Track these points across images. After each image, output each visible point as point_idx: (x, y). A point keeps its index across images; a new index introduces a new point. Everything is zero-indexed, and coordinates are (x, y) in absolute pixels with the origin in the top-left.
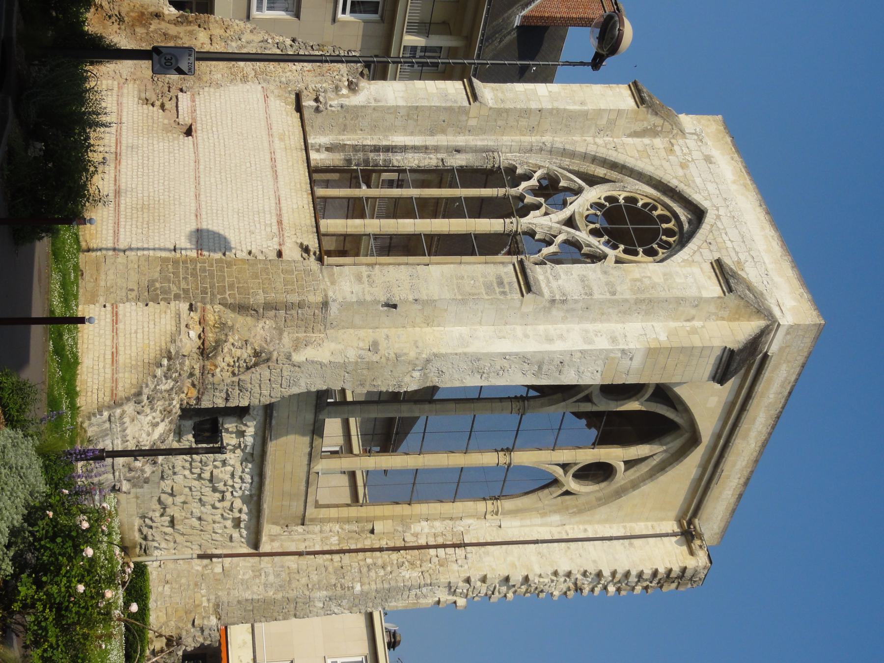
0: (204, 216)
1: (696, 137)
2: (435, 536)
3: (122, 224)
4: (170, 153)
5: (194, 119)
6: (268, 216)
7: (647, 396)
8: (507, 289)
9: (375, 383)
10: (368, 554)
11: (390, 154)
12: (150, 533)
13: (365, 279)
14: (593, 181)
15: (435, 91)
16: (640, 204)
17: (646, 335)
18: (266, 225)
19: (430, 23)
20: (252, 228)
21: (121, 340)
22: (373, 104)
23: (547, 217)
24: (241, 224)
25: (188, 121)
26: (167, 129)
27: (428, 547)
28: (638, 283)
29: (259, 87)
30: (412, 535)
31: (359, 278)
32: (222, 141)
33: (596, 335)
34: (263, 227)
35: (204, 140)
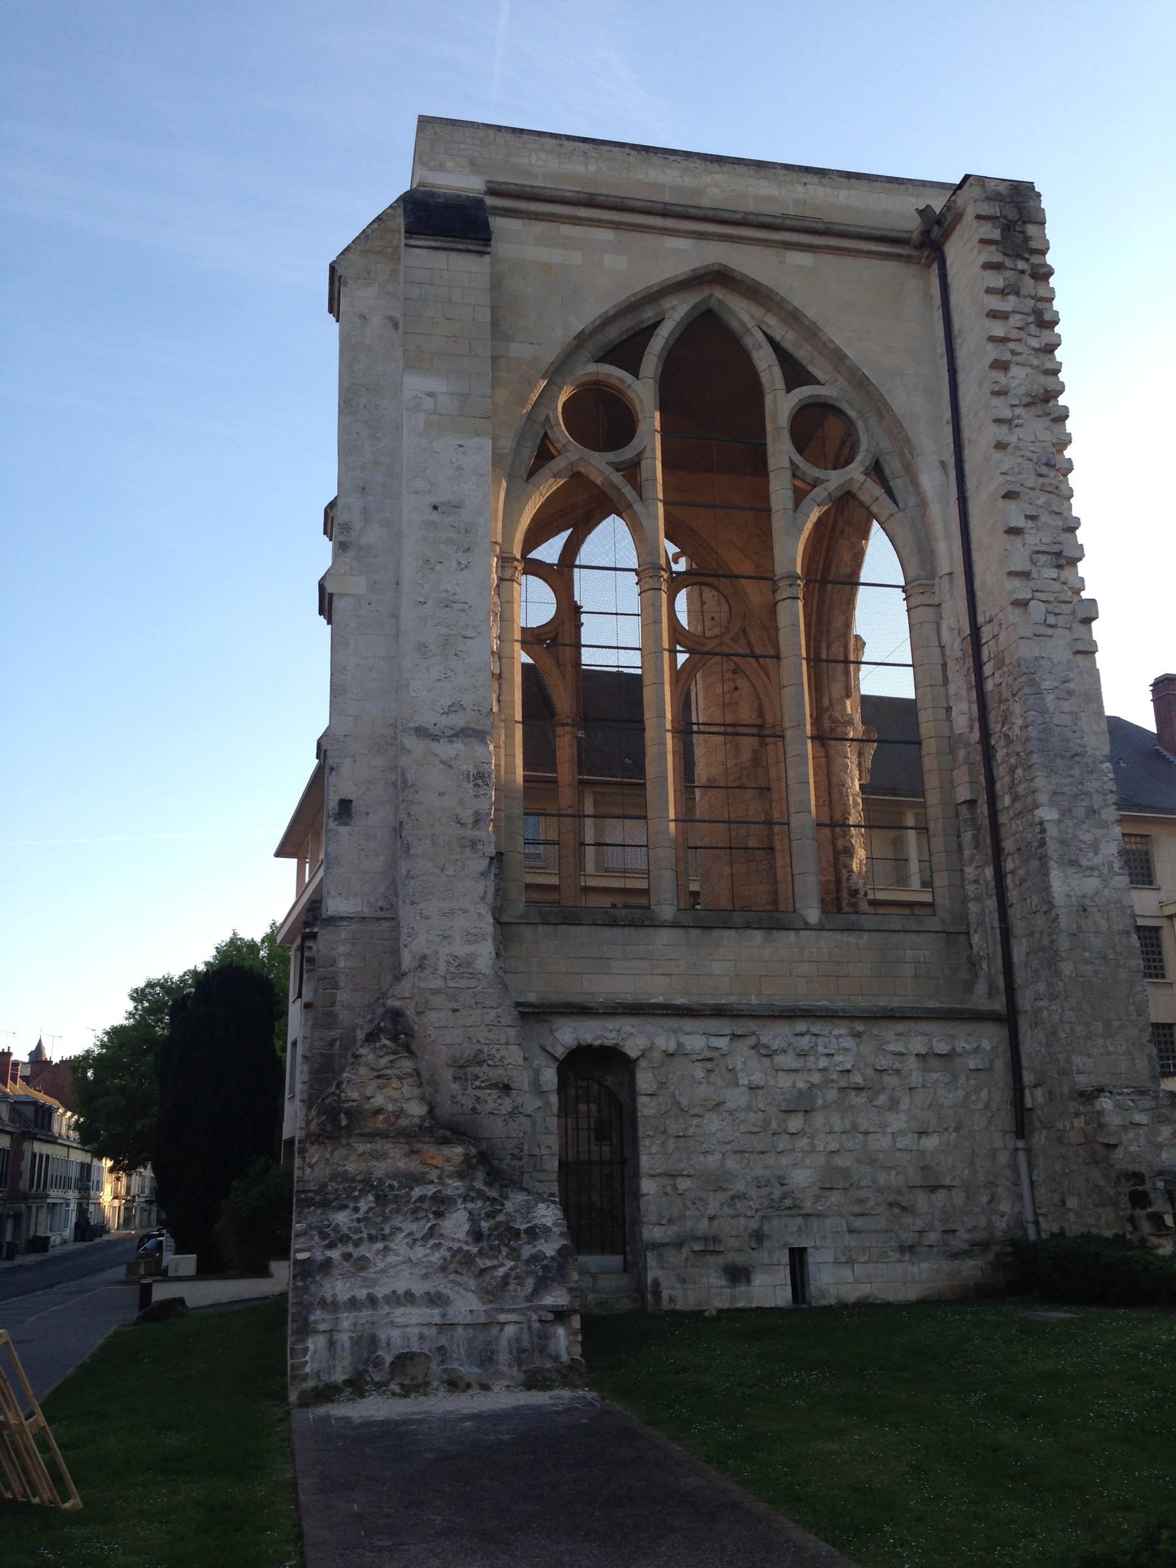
9: (470, 821)
12: (965, 1236)
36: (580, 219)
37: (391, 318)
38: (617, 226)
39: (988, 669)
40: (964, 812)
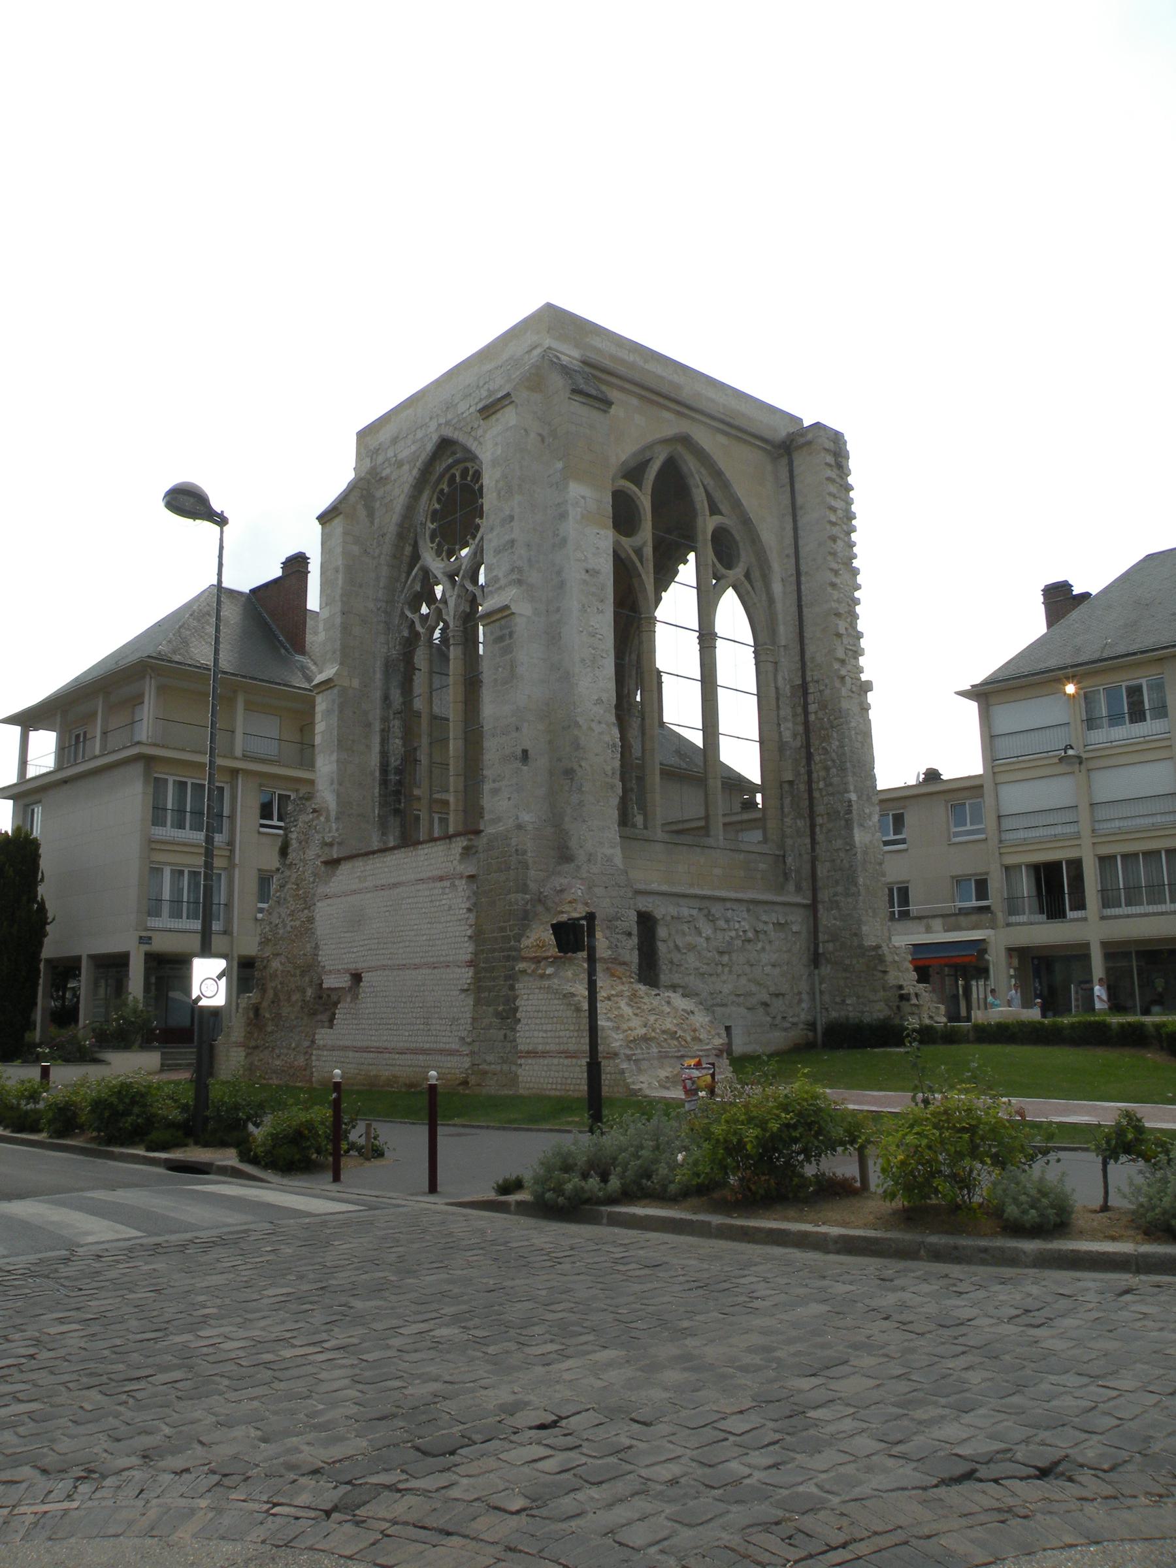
0: (435, 959)
1: (374, 456)
2: (795, 715)
3: (442, 1046)
4: (376, 996)
5: (347, 971)
6: (436, 892)
7: (635, 488)
8: (506, 632)
9: (610, 773)
10: (814, 786)
11: (390, 768)
13: (496, 785)
14: (416, 557)
15: (324, 723)
16: (437, 506)
17: (557, 483)
18: (443, 894)
19: (302, 743)
20: (446, 907)
21: (553, 1047)
22: (335, 786)
23: (449, 602)
24: (443, 919)
25: (347, 977)
26: (355, 997)
27: (806, 724)
28: (503, 493)
29: (319, 904)
30: (794, 740)
31: (495, 792)
32: (366, 942)
33: (558, 535)
34: (445, 897)
35: (364, 961)
36: (625, 388)
37: (540, 435)
38: (679, 413)
39: (812, 708)
40: (786, 787)
